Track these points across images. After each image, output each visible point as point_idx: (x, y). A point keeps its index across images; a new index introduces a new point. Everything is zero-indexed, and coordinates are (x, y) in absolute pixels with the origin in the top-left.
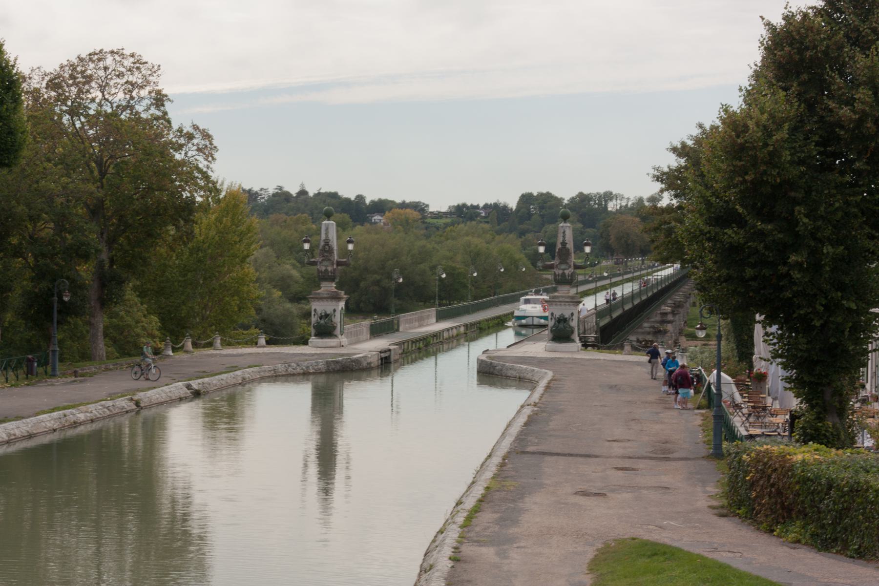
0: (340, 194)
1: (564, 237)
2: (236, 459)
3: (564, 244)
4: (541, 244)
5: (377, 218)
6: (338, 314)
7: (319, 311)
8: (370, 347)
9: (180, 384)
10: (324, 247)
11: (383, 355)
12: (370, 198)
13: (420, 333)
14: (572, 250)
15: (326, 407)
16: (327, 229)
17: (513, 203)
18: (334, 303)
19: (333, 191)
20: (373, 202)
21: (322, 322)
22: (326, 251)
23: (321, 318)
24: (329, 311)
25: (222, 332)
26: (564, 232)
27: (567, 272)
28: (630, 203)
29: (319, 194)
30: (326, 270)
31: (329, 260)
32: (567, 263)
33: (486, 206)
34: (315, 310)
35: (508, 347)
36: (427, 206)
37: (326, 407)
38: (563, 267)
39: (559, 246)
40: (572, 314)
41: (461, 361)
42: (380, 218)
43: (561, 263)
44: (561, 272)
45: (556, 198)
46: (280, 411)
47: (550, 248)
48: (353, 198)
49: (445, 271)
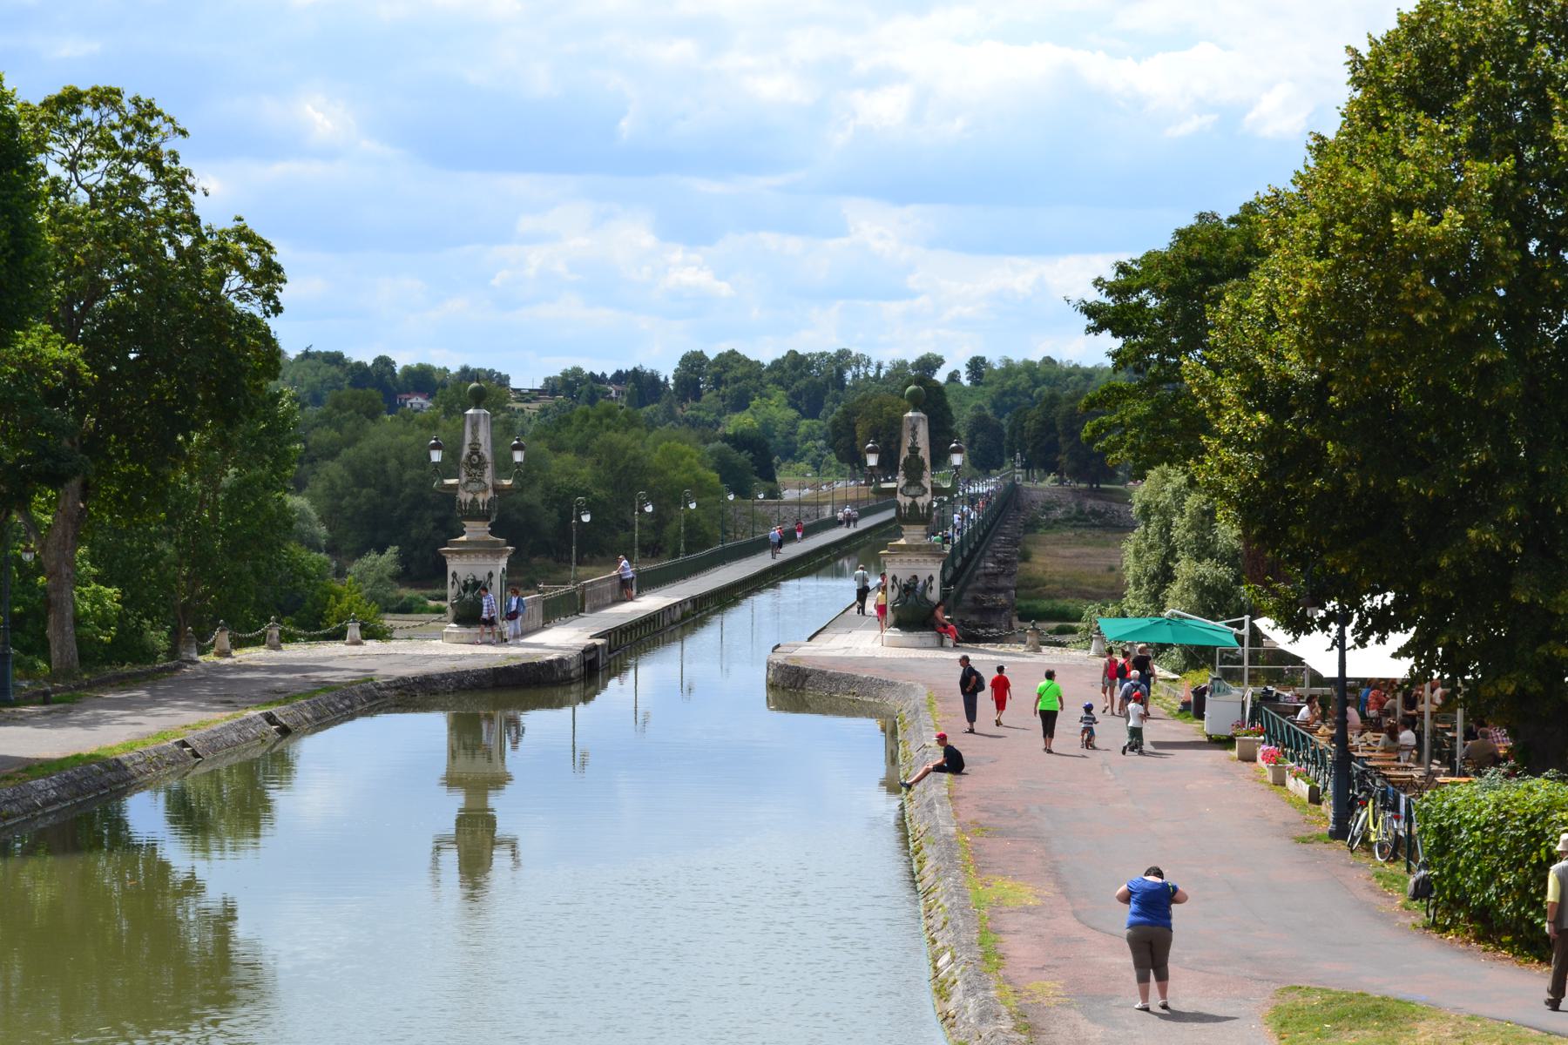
0: (346, 356)
2: (332, 861)
3: (914, 450)
4: (436, 447)
5: (417, 401)
7: (462, 577)
8: (563, 639)
9: (252, 713)
10: (469, 457)
11: (588, 658)
12: (403, 360)
13: (622, 615)
14: (927, 462)
15: (476, 772)
17: (667, 369)
18: (489, 561)
19: (332, 350)
20: (408, 371)
21: (468, 596)
22: (473, 466)
23: (465, 590)
24: (481, 575)
25: (231, 623)
27: (920, 501)
28: (883, 373)
29: (306, 355)
30: (474, 500)
32: (921, 485)
33: (619, 377)
34: (454, 575)
35: (810, 639)
36: (507, 378)
37: (476, 772)
38: (913, 491)
39: (466, 451)
40: (491, 575)
41: (728, 660)
42: (421, 400)
43: (908, 485)
44: (470, 497)
45: (748, 361)
46: (363, 780)
47: (452, 453)
48: (370, 363)
49: (1548, 472)
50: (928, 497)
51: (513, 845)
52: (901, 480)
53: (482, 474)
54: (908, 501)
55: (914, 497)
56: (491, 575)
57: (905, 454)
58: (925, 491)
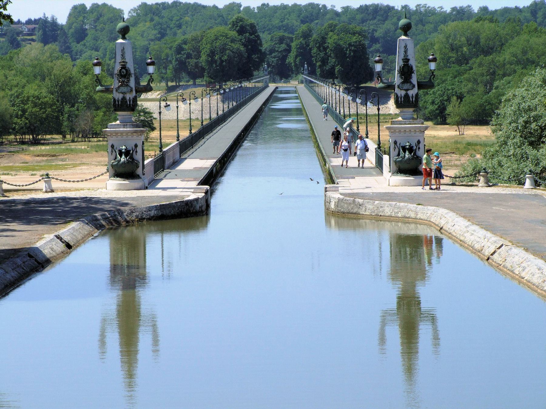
1: (406, 52)
3: (406, 60)
6: (139, 149)
16: (406, 47)
26: (406, 47)
30: (124, 98)
31: (127, 85)
32: (411, 83)
38: (406, 86)
40: (136, 146)
43: (402, 83)
45: (204, 7)
50: (416, 90)
51: (433, 319)
52: (397, 80)
53: (129, 81)
54: (403, 93)
55: (407, 90)
56: (136, 146)
57: (398, 63)
58: (414, 86)
